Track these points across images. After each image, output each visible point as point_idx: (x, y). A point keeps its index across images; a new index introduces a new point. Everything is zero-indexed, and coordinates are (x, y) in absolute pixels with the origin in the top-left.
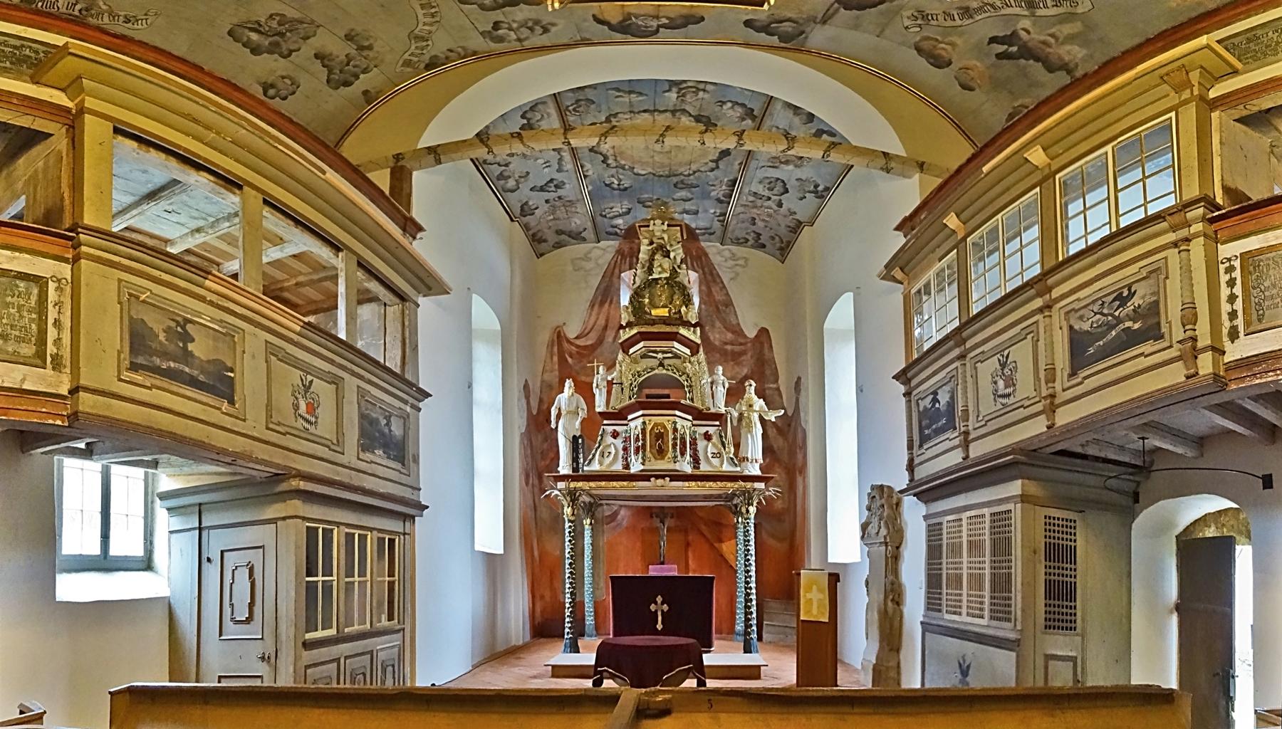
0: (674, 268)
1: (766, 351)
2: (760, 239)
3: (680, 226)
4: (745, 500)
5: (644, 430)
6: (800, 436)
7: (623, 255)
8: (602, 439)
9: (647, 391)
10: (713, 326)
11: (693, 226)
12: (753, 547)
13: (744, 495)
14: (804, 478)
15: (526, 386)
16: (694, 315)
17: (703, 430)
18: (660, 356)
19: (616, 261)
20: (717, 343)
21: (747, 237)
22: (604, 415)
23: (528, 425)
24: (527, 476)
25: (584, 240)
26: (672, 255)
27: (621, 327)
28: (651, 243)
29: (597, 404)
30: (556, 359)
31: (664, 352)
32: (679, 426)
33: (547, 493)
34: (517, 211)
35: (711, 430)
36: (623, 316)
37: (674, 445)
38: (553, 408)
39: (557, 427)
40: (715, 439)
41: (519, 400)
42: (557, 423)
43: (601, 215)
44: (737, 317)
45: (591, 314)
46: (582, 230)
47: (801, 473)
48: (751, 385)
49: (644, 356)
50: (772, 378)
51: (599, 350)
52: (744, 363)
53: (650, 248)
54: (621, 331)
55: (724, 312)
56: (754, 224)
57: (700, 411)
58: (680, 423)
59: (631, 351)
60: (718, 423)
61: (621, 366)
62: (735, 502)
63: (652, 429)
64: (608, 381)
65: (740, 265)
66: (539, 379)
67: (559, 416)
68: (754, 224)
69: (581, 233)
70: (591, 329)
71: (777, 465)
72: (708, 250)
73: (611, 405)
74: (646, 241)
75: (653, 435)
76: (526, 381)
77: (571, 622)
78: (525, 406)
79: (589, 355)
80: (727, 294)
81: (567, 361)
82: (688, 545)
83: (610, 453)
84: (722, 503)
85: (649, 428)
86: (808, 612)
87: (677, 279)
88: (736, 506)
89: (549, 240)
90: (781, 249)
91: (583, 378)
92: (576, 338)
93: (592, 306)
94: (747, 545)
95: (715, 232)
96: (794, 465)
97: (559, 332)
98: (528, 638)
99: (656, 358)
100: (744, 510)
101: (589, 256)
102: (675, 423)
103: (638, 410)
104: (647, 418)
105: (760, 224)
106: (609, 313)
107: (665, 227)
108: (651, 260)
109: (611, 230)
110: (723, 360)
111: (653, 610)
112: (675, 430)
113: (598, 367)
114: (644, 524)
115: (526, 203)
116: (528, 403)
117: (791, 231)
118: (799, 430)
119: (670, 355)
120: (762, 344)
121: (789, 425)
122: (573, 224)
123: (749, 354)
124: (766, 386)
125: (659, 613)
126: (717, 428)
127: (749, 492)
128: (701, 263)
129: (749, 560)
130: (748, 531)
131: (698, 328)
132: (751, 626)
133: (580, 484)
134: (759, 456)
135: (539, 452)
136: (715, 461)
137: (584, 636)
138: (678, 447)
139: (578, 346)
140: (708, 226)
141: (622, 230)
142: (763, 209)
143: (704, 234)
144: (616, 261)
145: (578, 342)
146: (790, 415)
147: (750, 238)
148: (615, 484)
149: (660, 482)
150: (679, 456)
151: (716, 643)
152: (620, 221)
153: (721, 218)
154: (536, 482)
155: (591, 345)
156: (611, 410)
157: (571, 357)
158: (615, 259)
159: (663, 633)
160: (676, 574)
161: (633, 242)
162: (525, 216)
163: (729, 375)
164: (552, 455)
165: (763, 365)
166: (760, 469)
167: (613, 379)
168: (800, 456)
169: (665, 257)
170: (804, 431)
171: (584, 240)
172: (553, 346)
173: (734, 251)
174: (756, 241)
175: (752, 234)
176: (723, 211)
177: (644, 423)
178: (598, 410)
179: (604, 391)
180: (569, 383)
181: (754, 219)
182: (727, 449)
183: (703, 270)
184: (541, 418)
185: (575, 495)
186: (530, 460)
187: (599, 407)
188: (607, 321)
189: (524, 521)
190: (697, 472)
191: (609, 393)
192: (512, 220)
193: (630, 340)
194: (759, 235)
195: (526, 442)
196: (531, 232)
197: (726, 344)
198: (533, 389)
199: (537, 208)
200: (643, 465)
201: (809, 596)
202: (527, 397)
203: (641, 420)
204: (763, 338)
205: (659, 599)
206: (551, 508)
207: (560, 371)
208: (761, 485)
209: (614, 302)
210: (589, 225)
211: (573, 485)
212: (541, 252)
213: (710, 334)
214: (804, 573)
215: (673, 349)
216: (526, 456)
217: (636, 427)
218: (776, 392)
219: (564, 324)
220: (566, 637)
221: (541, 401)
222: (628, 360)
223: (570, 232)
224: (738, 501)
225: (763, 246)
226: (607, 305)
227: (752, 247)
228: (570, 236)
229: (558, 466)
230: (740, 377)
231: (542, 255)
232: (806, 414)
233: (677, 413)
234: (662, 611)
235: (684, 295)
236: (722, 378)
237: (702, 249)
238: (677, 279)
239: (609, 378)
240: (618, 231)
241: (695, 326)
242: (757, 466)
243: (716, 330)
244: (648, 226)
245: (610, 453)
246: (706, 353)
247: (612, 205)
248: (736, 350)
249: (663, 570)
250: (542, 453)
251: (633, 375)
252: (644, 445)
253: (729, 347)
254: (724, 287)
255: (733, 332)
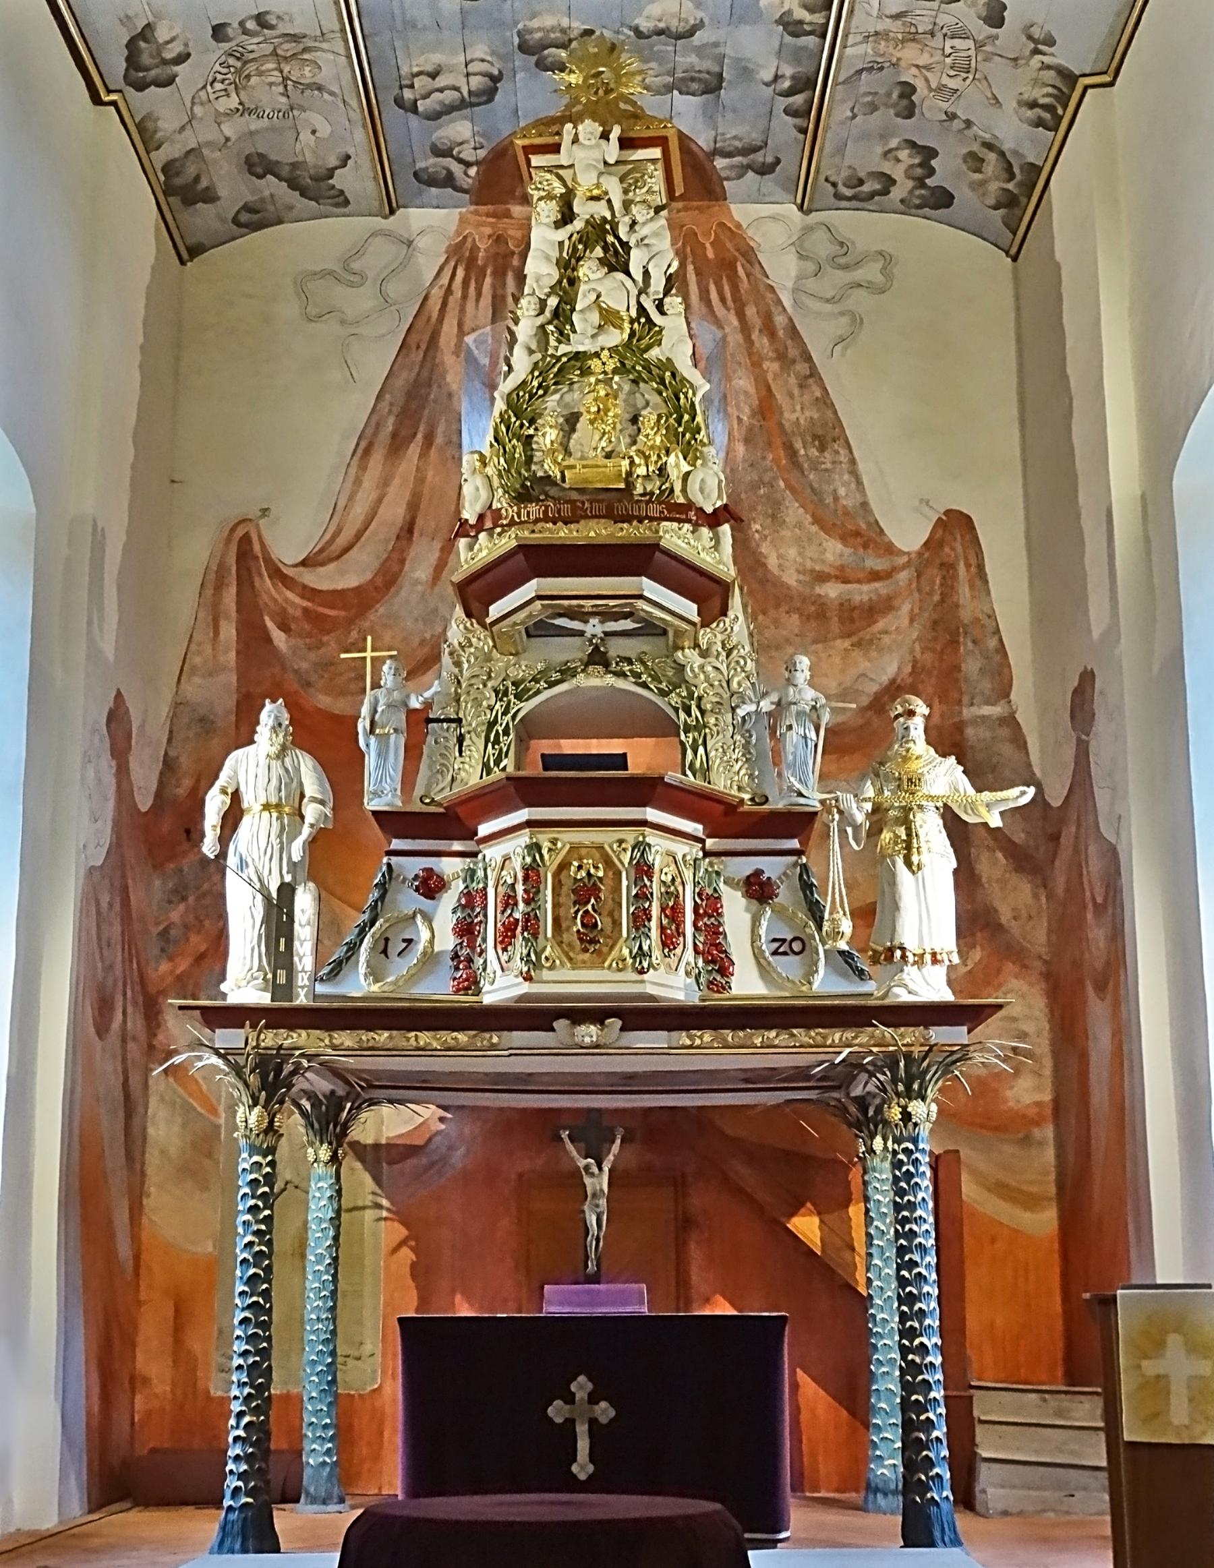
0: (642, 310)
1: (964, 593)
2: (931, 172)
3: (662, 142)
4: (895, 1080)
5: (532, 874)
6: (1095, 865)
7: (471, 263)
8: (382, 897)
9: (547, 746)
10: (775, 518)
11: (703, 140)
12: (929, 1225)
13: (894, 1066)
14: (1116, 1005)
15: (117, 717)
16: (712, 484)
17: (745, 867)
18: (594, 627)
19: (449, 291)
20: (791, 578)
21: (887, 167)
22: (391, 821)
23: (116, 847)
24: (104, 1007)
25: (341, 200)
26: (636, 261)
27: (464, 529)
28: (567, 217)
29: (369, 786)
30: (229, 631)
31: (607, 615)
32: (656, 859)
33: (177, 1059)
34: (115, 64)
35: (772, 867)
36: (467, 490)
37: (640, 919)
38: (214, 791)
39: (222, 855)
40: (785, 895)
41: (87, 759)
42: (225, 839)
43: (399, 102)
44: (859, 483)
45: (358, 482)
46: (333, 161)
47: (1101, 988)
48: (911, 713)
49: (540, 630)
50: (986, 685)
51: (381, 609)
52: (886, 640)
53: (562, 234)
54: (462, 543)
55: (815, 465)
56: (909, 112)
57: (730, 808)
58: (659, 844)
59: (496, 610)
60: (794, 844)
61: (458, 664)
62: (857, 1091)
63: (564, 866)
64: (411, 712)
65: (869, 286)
66: (167, 695)
67: (233, 817)
68: (909, 112)
69: (331, 173)
70: (358, 536)
71: (1010, 967)
72: (755, 236)
73: (419, 791)
74: (547, 211)
75: (568, 885)
76: (119, 695)
77: (248, 1458)
78: (110, 781)
79: (350, 622)
80: (825, 401)
81: (269, 640)
82: (685, 1223)
83: (409, 941)
84: (812, 1095)
85: (551, 863)
86: (1155, 1416)
87: (654, 354)
88: (862, 1103)
89: (223, 191)
90: (1009, 202)
91: (324, 701)
92: (304, 563)
93: (364, 451)
94: (905, 1221)
95: (778, 161)
96: (1077, 964)
97: (246, 540)
98: (76, 1508)
99: (581, 633)
100: (895, 1113)
101: (356, 266)
102: (642, 847)
103: (517, 808)
104: (544, 838)
105: (931, 106)
106: (420, 480)
107: (612, 151)
108: (567, 285)
109: (429, 163)
110: (811, 635)
111: (559, 1420)
112: (643, 870)
113: (377, 663)
114: (527, 1162)
115: (147, 33)
116: (122, 771)
117: (1039, 123)
118: (1092, 849)
119: (628, 625)
120: (948, 568)
121: (1055, 838)
122: (305, 136)
123: (906, 608)
124: (967, 713)
125: (582, 1429)
126: (791, 859)
127: (908, 1056)
128: (735, 288)
129: (913, 1264)
130: (909, 1176)
131: (726, 529)
132: (930, 1463)
133: (299, 1038)
134: (944, 937)
135: (155, 930)
136: (787, 966)
137: (297, 1501)
138: (654, 924)
139: (310, 593)
140: (756, 137)
141: (468, 164)
142: (937, 41)
143: (742, 170)
144: (449, 291)
145: (310, 578)
146: (1056, 803)
147: (898, 173)
148: (425, 1038)
149: (589, 1033)
150: (657, 954)
151: (798, 1516)
152: (459, 129)
153: (799, 99)
154: (136, 1024)
155: (357, 590)
156: (417, 807)
157: (284, 627)
158: (445, 280)
159: (587, 1486)
160: (645, 1310)
161: (508, 215)
162: (140, 87)
163: (833, 686)
164: (198, 943)
165: (954, 643)
166: (950, 983)
167: (428, 705)
168: (1097, 935)
169: (612, 269)
170: (1112, 855)
171: (341, 200)
172: (219, 586)
173: (845, 232)
174: (920, 182)
175: (904, 154)
176: (805, 69)
177: (535, 848)
178: (372, 804)
179: (398, 743)
180: (270, 713)
181: (908, 90)
182: (826, 926)
183: (741, 315)
184: (167, 825)
185: (279, 1069)
186: (117, 956)
187: (376, 794)
188: (413, 507)
189: (110, 1502)
190: (718, 1000)
191: (413, 752)
192: (96, 100)
193: (490, 577)
194: (929, 153)
195: (105, 899)
196: (160, 157)
197: (822, 578)
198: (142, 726)
199: (182, 58)
200: (528, 978)
201: (1150, 1367)
202: (120, 751)
203: (524, 838)
204: (955, 549)
205: (581, 1386)
206: (188, 1109)
207: (242, 674)
208: (956, 1035)
209: (439, 440)
210: (360, 138)
211: (270, 1039)
212: (191, 241)
213: (764, 548)
214: (1123, 1296)
215: (641, 604)
216: (103, 943)
217: (507, 858)
218: (1004, 732)
219: (265, 512)
220: (227, 1502)
221: (169, 766)
222: (480, 639)
223: (294, 165)
224: (871, 1088)
225: (943, 199)
226: (414, 450)
227: (908, 207)
228: (293, 184)
229: (223, 978)
230: (873, 688)
231: (195, 251)
232: (1117, 792)
233: (652, 814)
234: (593, 1422)
235: (679, 410)
236: (810, 694)
237: (734, 233)
238: (654, 354)
239: (415, 703)
240: (457, 169)
241: (714, 520)
242: (940, 973)
243: (786, 533)
244: (555, 149)
245: (409, 941)
246: (751, 617)
247: (436, 58)
248: (857, 599)
249: (595, 1299)
250: (164, 934)
251: (501, 694)
252: (531, 924)
253: (832, 591)
254: (814, 373)
255: (850, 536)
